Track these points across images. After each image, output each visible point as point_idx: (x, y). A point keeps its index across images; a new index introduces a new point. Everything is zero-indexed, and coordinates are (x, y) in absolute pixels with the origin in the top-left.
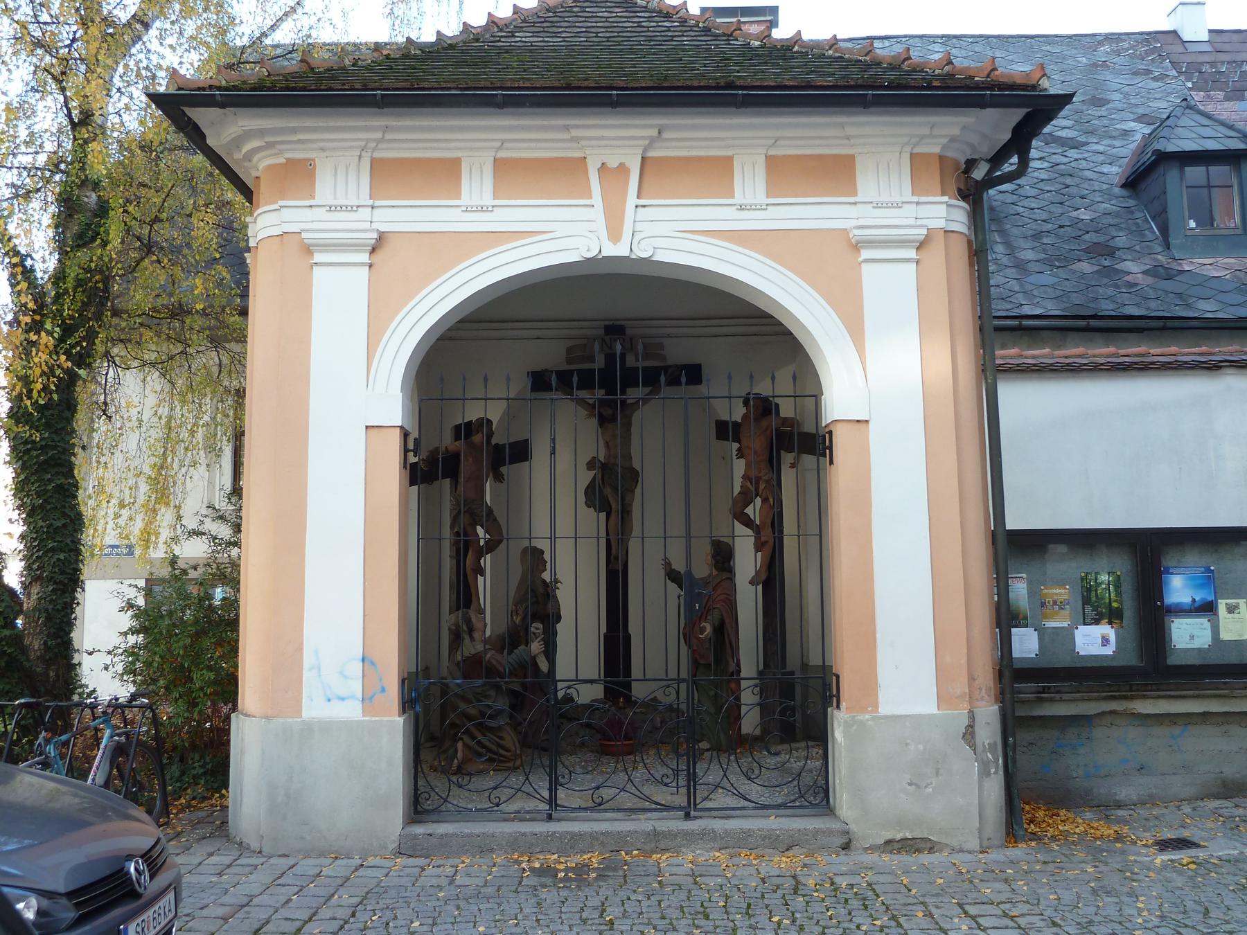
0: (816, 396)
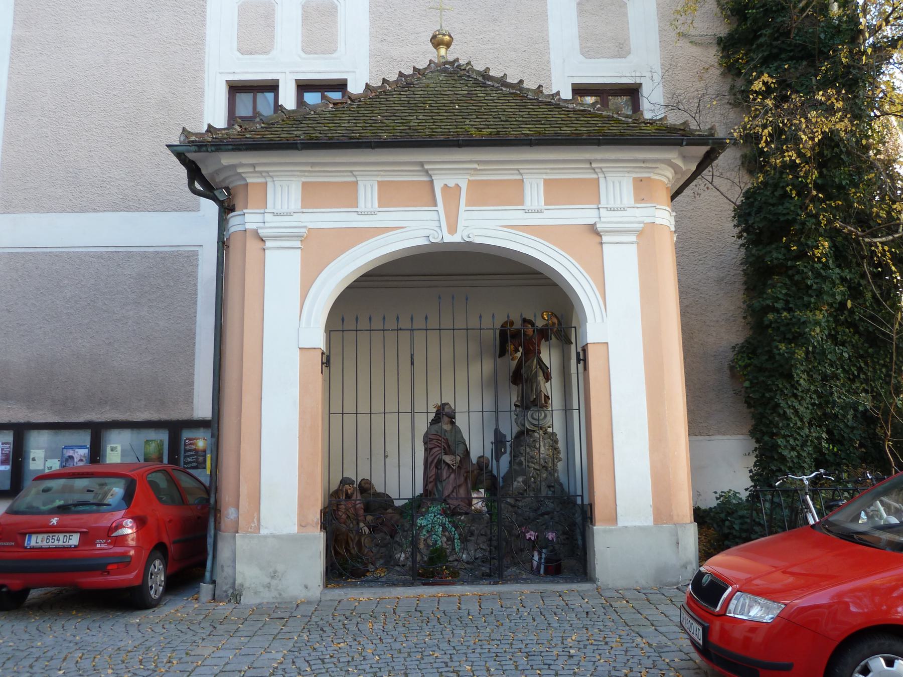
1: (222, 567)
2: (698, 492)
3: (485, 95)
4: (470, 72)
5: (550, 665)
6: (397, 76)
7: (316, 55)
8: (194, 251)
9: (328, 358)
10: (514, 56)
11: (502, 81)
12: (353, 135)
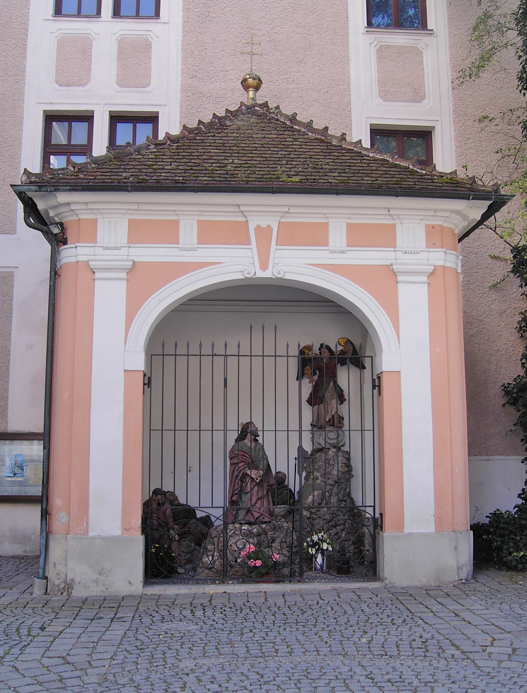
0: (372, 357)
1: (55, 564)
2: (476, 507)
3: (293, 140)
4: (279, 116)
5: (348, 638)
6: (211, 118)
7: (129, 89)
8: (10, 272)
9: (150, 379)
10: (317, 96)
11: (309, 125)
12: (177, 178)
